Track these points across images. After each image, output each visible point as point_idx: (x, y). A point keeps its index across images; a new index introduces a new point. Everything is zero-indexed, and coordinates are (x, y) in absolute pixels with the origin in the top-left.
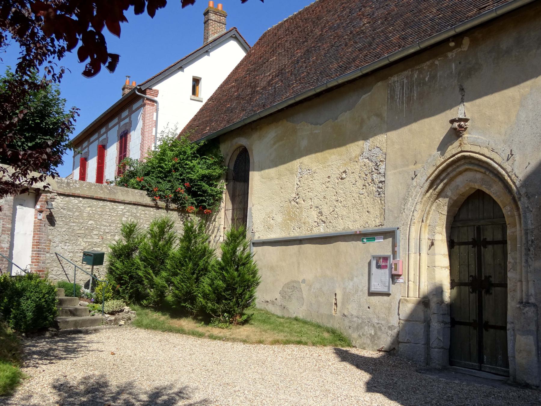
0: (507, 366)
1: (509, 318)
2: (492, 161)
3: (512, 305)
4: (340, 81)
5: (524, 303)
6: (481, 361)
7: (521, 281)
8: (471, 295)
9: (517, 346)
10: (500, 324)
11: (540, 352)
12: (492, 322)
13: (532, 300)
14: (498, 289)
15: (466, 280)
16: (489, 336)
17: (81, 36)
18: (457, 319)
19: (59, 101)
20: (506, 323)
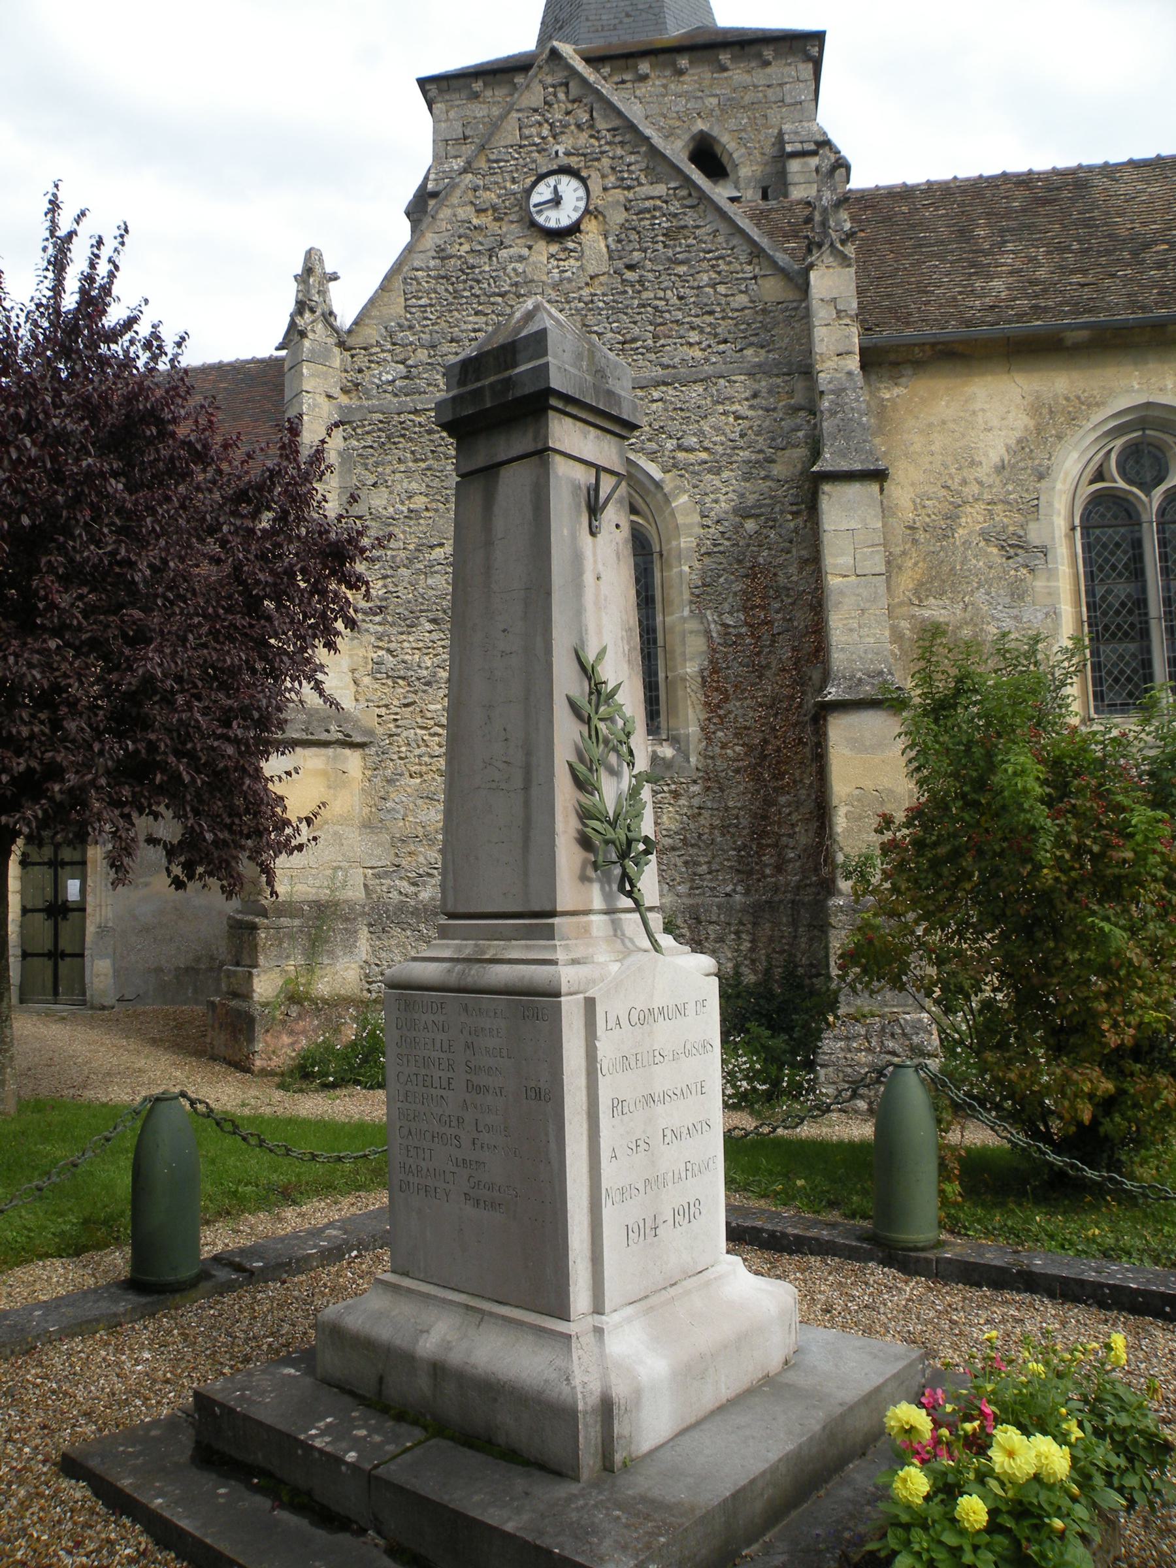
0: (84, 994)
1: (88, 943)
2: (582, 1081)
3: (91, 929)
4: (794, 1514)
5: (103, 930)
6: (56, 993)
7: (100, 905)
8: (46, 923)
9: (95, 970)
10: (77, 951)
11: (408, 1444)
12: (68, 950)
13: (110, 924)
14: (76, 914)
15: (40, 904)
16: (65, 966)
17: (4, 733)
18: (29, 951)
19: (288, 831)
20: (83, 949)
